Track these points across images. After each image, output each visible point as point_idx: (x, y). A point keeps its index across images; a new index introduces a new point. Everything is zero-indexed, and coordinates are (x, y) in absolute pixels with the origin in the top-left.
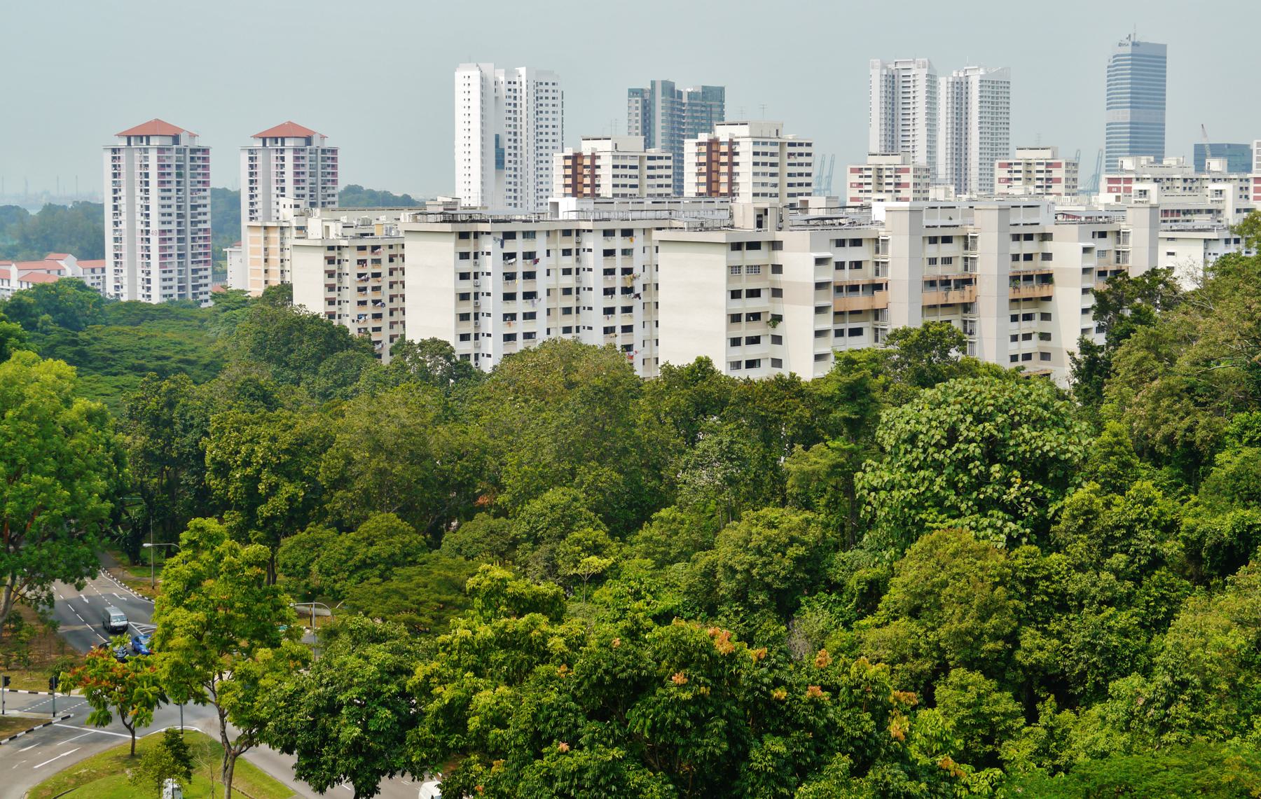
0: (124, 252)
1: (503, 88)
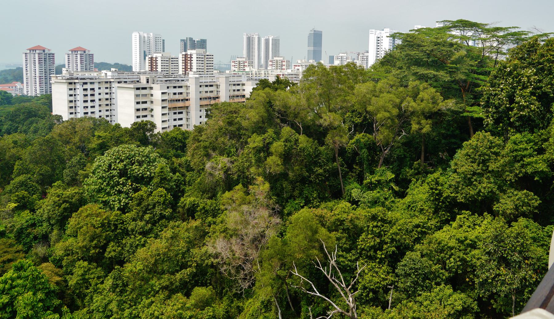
0: (29, 82)
1: (146, 38)
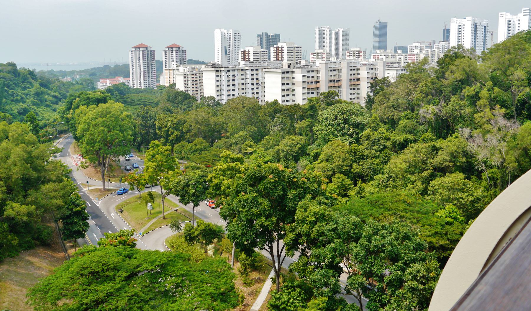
1: (226, 35)
